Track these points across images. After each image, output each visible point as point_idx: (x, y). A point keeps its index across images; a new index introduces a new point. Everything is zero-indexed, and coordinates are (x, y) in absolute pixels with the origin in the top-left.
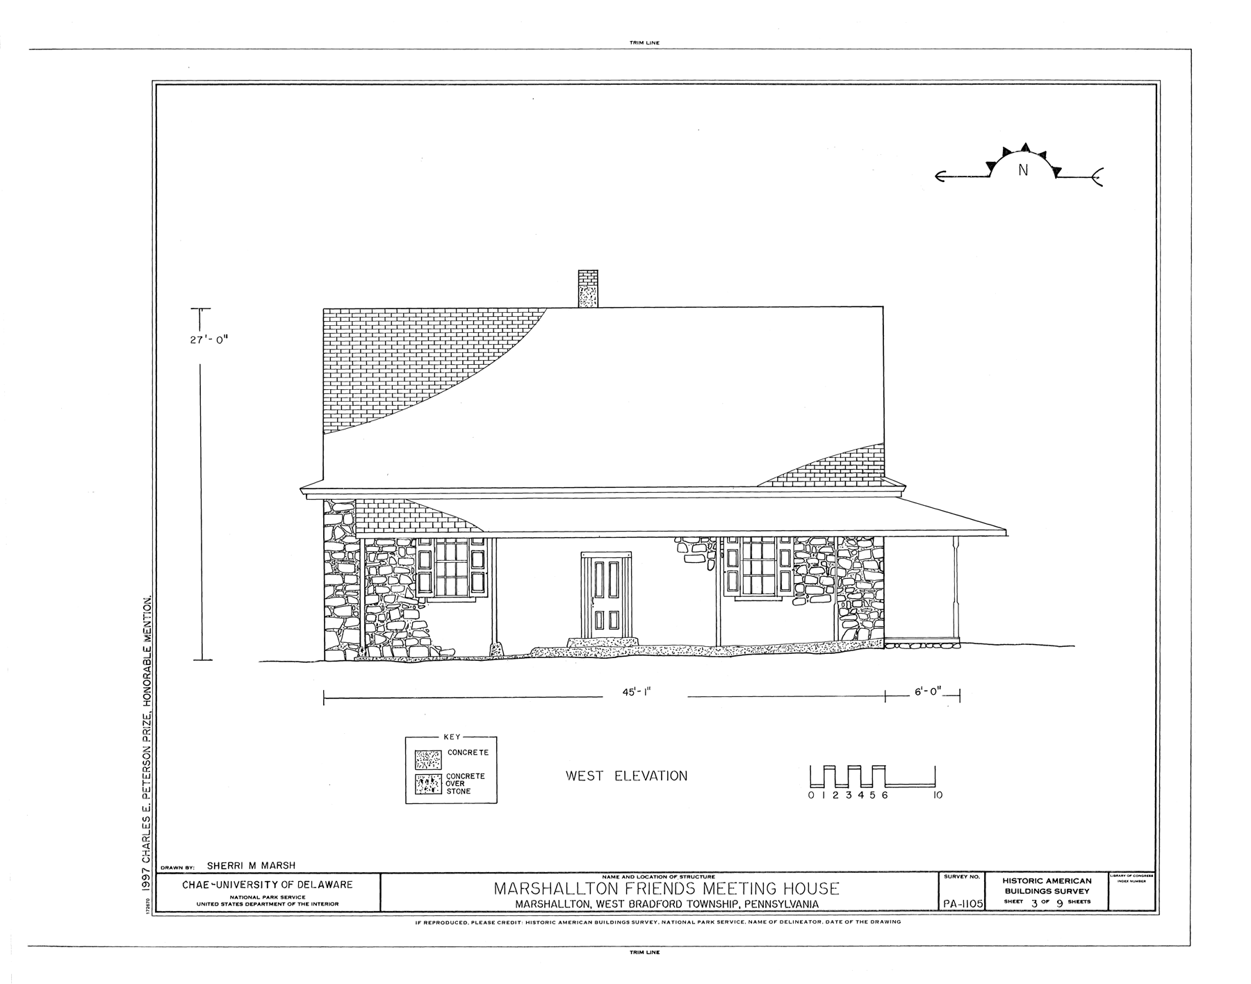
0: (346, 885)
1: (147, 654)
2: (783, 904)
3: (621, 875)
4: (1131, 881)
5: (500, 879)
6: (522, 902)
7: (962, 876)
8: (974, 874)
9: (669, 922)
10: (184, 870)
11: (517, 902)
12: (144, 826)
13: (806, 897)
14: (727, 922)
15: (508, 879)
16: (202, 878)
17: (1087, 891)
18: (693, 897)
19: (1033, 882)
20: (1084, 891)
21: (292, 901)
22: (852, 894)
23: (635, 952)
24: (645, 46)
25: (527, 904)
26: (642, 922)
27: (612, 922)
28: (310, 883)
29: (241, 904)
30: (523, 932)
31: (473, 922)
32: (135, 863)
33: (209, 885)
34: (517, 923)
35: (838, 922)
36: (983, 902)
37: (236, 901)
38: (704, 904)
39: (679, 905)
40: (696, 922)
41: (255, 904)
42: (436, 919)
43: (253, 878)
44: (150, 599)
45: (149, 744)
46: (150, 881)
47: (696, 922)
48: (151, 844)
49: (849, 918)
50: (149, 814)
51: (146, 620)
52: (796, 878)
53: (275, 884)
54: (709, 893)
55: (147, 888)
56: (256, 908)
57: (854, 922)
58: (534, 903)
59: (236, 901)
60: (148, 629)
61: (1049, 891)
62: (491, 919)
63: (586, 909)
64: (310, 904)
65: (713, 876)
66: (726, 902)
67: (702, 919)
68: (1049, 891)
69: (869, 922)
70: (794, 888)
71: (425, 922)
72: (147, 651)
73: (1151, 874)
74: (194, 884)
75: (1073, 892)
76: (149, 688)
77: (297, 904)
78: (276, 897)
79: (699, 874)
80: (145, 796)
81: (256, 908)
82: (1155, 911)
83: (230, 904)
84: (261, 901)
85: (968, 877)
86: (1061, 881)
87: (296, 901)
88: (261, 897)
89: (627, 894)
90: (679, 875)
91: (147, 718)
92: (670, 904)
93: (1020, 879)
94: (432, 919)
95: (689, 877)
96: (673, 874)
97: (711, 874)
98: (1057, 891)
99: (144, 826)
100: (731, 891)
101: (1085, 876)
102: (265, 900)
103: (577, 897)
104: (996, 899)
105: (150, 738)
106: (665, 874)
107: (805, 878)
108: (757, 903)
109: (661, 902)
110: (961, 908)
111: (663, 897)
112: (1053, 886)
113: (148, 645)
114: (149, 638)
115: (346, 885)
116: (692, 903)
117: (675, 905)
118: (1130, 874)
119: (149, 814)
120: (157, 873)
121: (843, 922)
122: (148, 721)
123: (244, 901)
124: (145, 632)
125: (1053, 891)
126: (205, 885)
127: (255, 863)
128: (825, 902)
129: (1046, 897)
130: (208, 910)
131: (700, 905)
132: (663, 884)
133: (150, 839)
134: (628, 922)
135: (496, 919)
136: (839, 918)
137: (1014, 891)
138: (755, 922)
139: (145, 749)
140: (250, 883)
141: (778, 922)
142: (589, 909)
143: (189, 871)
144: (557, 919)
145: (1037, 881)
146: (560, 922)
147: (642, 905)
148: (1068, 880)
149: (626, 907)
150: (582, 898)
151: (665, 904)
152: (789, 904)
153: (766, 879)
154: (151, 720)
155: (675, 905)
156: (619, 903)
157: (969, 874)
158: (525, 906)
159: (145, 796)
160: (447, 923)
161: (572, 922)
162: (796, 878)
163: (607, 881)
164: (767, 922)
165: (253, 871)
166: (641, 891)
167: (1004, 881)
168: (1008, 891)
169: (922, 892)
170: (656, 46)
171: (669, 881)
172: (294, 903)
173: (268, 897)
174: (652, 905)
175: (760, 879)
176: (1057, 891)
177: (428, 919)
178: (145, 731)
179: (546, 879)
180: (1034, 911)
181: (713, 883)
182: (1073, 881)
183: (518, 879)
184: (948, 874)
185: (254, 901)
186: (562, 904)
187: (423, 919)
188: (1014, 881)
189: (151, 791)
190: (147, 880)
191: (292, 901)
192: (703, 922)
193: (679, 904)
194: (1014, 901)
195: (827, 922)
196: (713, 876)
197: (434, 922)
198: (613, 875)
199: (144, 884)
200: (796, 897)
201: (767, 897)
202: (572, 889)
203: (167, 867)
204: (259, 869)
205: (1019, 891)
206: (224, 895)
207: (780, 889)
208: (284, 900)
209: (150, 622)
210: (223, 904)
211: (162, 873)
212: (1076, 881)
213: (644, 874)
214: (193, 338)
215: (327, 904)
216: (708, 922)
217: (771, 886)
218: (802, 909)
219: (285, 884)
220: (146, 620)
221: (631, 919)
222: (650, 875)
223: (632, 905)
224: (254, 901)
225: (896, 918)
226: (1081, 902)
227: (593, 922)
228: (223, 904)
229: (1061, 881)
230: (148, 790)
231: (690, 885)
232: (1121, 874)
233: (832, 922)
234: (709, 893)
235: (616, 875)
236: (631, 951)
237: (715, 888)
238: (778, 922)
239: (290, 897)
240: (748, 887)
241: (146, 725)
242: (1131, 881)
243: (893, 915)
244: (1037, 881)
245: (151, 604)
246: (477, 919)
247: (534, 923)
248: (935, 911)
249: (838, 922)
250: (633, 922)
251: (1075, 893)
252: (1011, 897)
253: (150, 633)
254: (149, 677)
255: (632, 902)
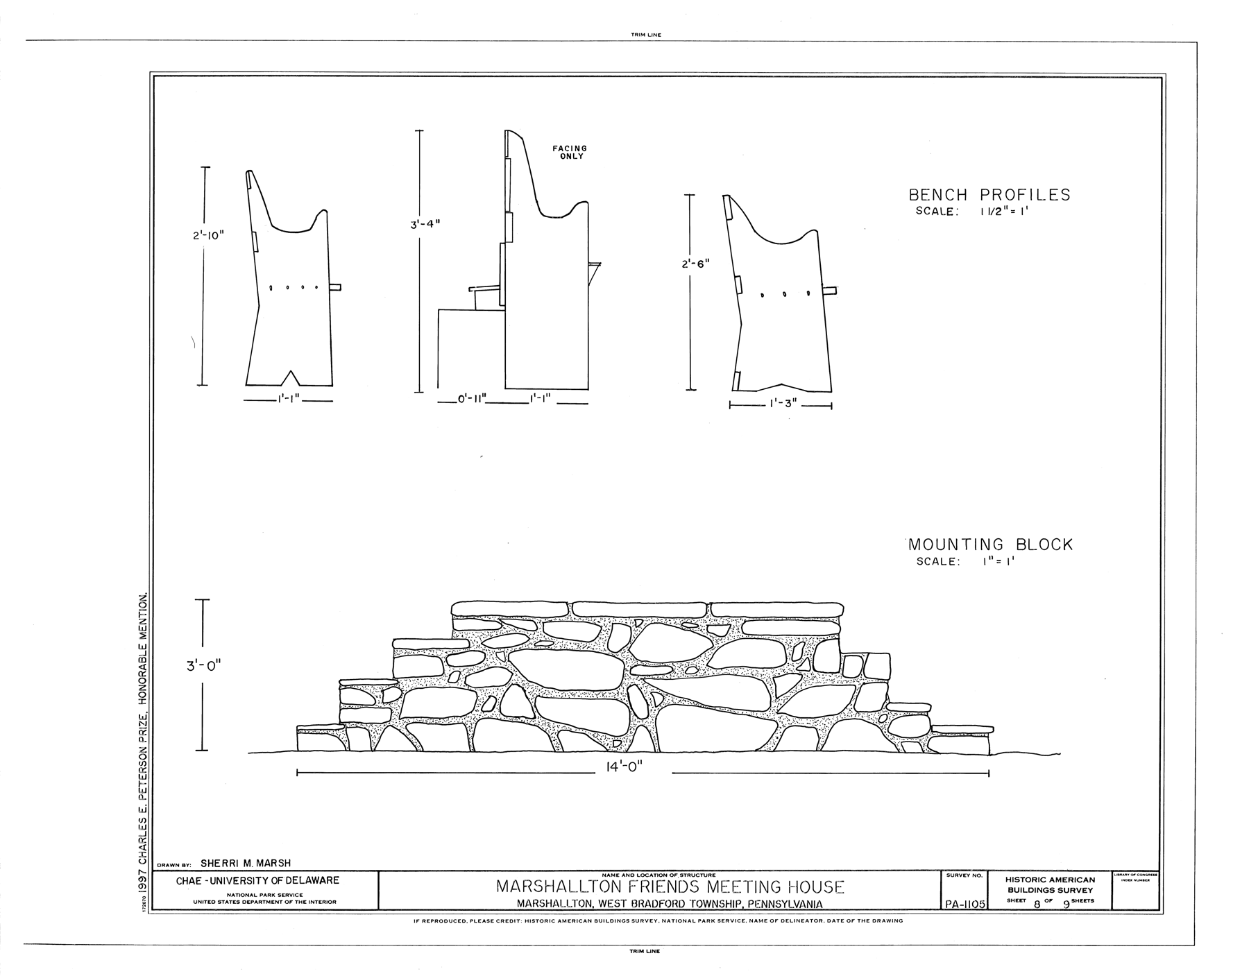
0: (333, 881)
1: (143, 652)
2: (787, 904)
3: (621, 873)
4: (1135, 880)
5: (503, 877)
6: (262, 861)
7: (964, 875)
8: (977, 873)
9: (669, 921)
10: (181, 868)
11: (258, 860)
12: (141, 647)
13: (811, 897)
14: (728, 921)
15: (511, 877)
16: (195, 875)
17: (1090, 890)
18: (697, 897)
19: (1036, 880)
20: (1088, 890)
21: (289, 898)
22: (856, 892)
23: (635, 951)
24: (646, 38)
25: (528, 903)
26: (642, 921)
27: (612, 921)
28: (298, 879)
29: (238, 902)
30: (522, 931)
31: (471, 921)
32: (132, 866)
33: (202, 881)
34: (517, 921)
35: (840, 921)
36: (986, 903)
37: (233, 898)
38: (707, 903)
39: (682, 905)
40: (696, 920)
41: (252, 902)
42: (434, 917)
43: (246, 875)
44: (145, 596)
45: (146, 745)
46: (146, 883)
47: (696, 920)
48: (822, 285)
49: (851, 917)
50: (145, 815)
51: (142, 617)
52: (801, 877)
53: (265, 880)
54: (713, 891)
55: (143, 889)
56: (253, 906)
57: (856, 921)
58: (536, 902)
59: (233, 898)
60: (144, 626)
61: (1052, 890)
62: (490, 917)
63: (588, 907)
64: (307, 902)
65: (713, 875)
66: (729, 902)
67: (702, 917)
68: (1052, 890)
69: (871, 921)
70: (798, 887)
71: (424, 921)
72: (142, 649)
73: (1155, 873)
74: (187, 881)
75: (1076, 891)
76: (145, 686)
77: (294, 902)
78: (273, 895)
79: (700, 872)
80: (141, 797)
81: (253, 906)
82: (1159, 910)
83: (227, 902)
84: (258, 899)
85: (971, 875)
86: (1064, 880)
87: (294, 899)
88: (258, 894)
89: (630, 893)
90: (679, 873)
91: (143, 779)
92: (672, 903)
93: (1023, 878)
94: (430, 917)
95: (689, 875)
96: (674, 872)
97: (712, 873)
98: (1061, 890)
99: (141, 647)
100: (735, 889)
101: (1088, 875)
102: (262, 898)
103: (580, 896)
104: (999, 898)
105: (146, 738)
106: (665, 873)
107: (809, 877)
108: (760, 903)
109: (664, 902)
110: (964, 907)
111: (666, 897)
112: (1057, 885)
113: (143, 642)
114: (145, 636)
115: (333, 881)
116: (695, 902)
117: (678, 904)
118: (1134, 873)
119: (145, 815)
120: (153, 871)
121: (845, 921)
122: (144, 721)
123: (241, 899)
124: (141, 629)
125: (1056, 890)
126: (196, 881)
127: (250, 861)
128: (828, 900)
129: (1049, 896)
130: (203, 907)
131: (703, 905)
132: (666, 882)
133: (146, 840)
134: (628, 921)
135: (495, 918)
136: (840, 917)
137: (1017, 890)
138: (756, 921)
139: (141, 597)
140: (243, 879)
141: (779, 921)
142: (592, 908)
143: (186, 868)
144: (557, 918)
145: (1041, 880)
146: (560, 921)
147: (644, 904)
148: (1071, 879)
149: (628, 905)
150: (585, 897)
151: (668, 904)
152: (792, 905)
153: (770, 877)
154: (147, 720)
155: (678, 904)
156: (621, 903)
157: (971, 873)
158: (646, 905)
159: (141, 797)
160: (446, 921)
161: (725, 921)
162: (801, 877)
163: (610, 879)
164: (768, 921)
165: (248, 868)
166: (644, 889)
167: (1007, 879)
168: (1011, 890)
169: (924, 891)
170: (658, 38)
171: (673, 880)
172: (291, 901)
173: (265, 895)
174: (655, 905)
175: (765, 877)
176: (1061, 890)
177: (426, 917)
178: (142, 732)
179: (549, 877)
180: (1037, 908)
181: (718, 882)
182: (1077, 880)
183: (520, 877)
184: (950, 872)
185: (251, 899)
186: (564, 904)
187: (421, 918)
188: (1017, 880)
189: (147, 791)
190: (143, 882)
191: (289, 898)
192: (704, 921)
193: (682, 904)
194: (1081, 900)
195: (829, 921)
196: (713, 875)
197: (432, 921)
198: (613, 873)
199: (141, 886)
200: (800, 897)
201: (771, 896)
202: (575, 887)
203: (163, 865)
204: (254, 866)
205: (1022, 890)
206: (220, 892)
207: (785, 887)
208: (281, 898)
209: (145, 620)
210: (219, 902)
211: (158, 871)
212: (1080, 880)
213: (645, 872)
214: (196, 234)
215: (324, 902)
216: (708, 921)
217: (776, 884)
218: (532, 908)
219: (275, 881)
220: (142, 617)
221: (631, 917)
222: (650, 873)
223: (634, 905)
224: (251, 899)
225: (898, 917)
226: (1085, 900)
227: (593, 921)
228: (219, 902)
229: (1064, 880)
230: (144, 791)
231: (694, 883)
232: (1124, 873)
233: (834, 921)
234: (713, 891)
235: (616, 873)
236: (631, 950)
237: (718, 886)
238: (779, 921)
239: (287, 895)
240: (752, 885)
241: (142, 726)
242: (1135, 880)
243: (894, 914)
244: (1041, 880)
245: (147, 602)
246: (476, 918)
247: (534, 921)
248: (938, 910)
249: (840, 921)
250: (633, 921)
251: (1079, 892)
252: (1014, 896)
253: (146, 630)
254: (144, 674)
255: (634, 902)
